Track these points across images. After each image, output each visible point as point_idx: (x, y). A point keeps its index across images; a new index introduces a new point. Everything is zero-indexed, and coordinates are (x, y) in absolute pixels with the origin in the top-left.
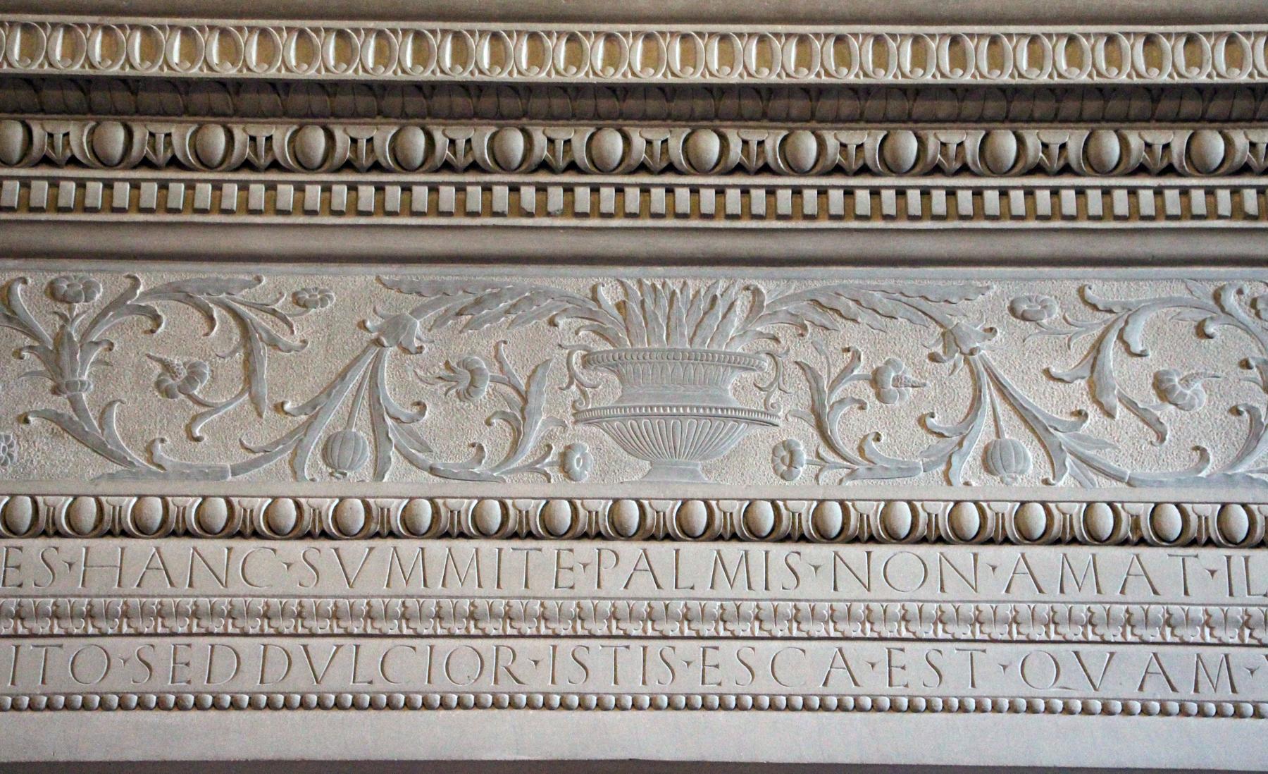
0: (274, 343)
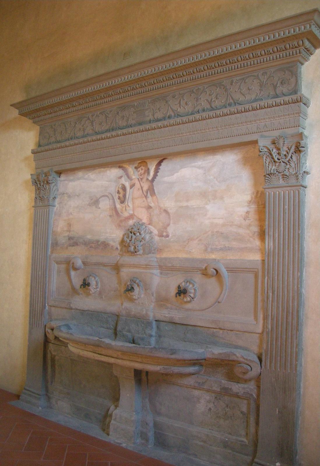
0: (108, 117)
